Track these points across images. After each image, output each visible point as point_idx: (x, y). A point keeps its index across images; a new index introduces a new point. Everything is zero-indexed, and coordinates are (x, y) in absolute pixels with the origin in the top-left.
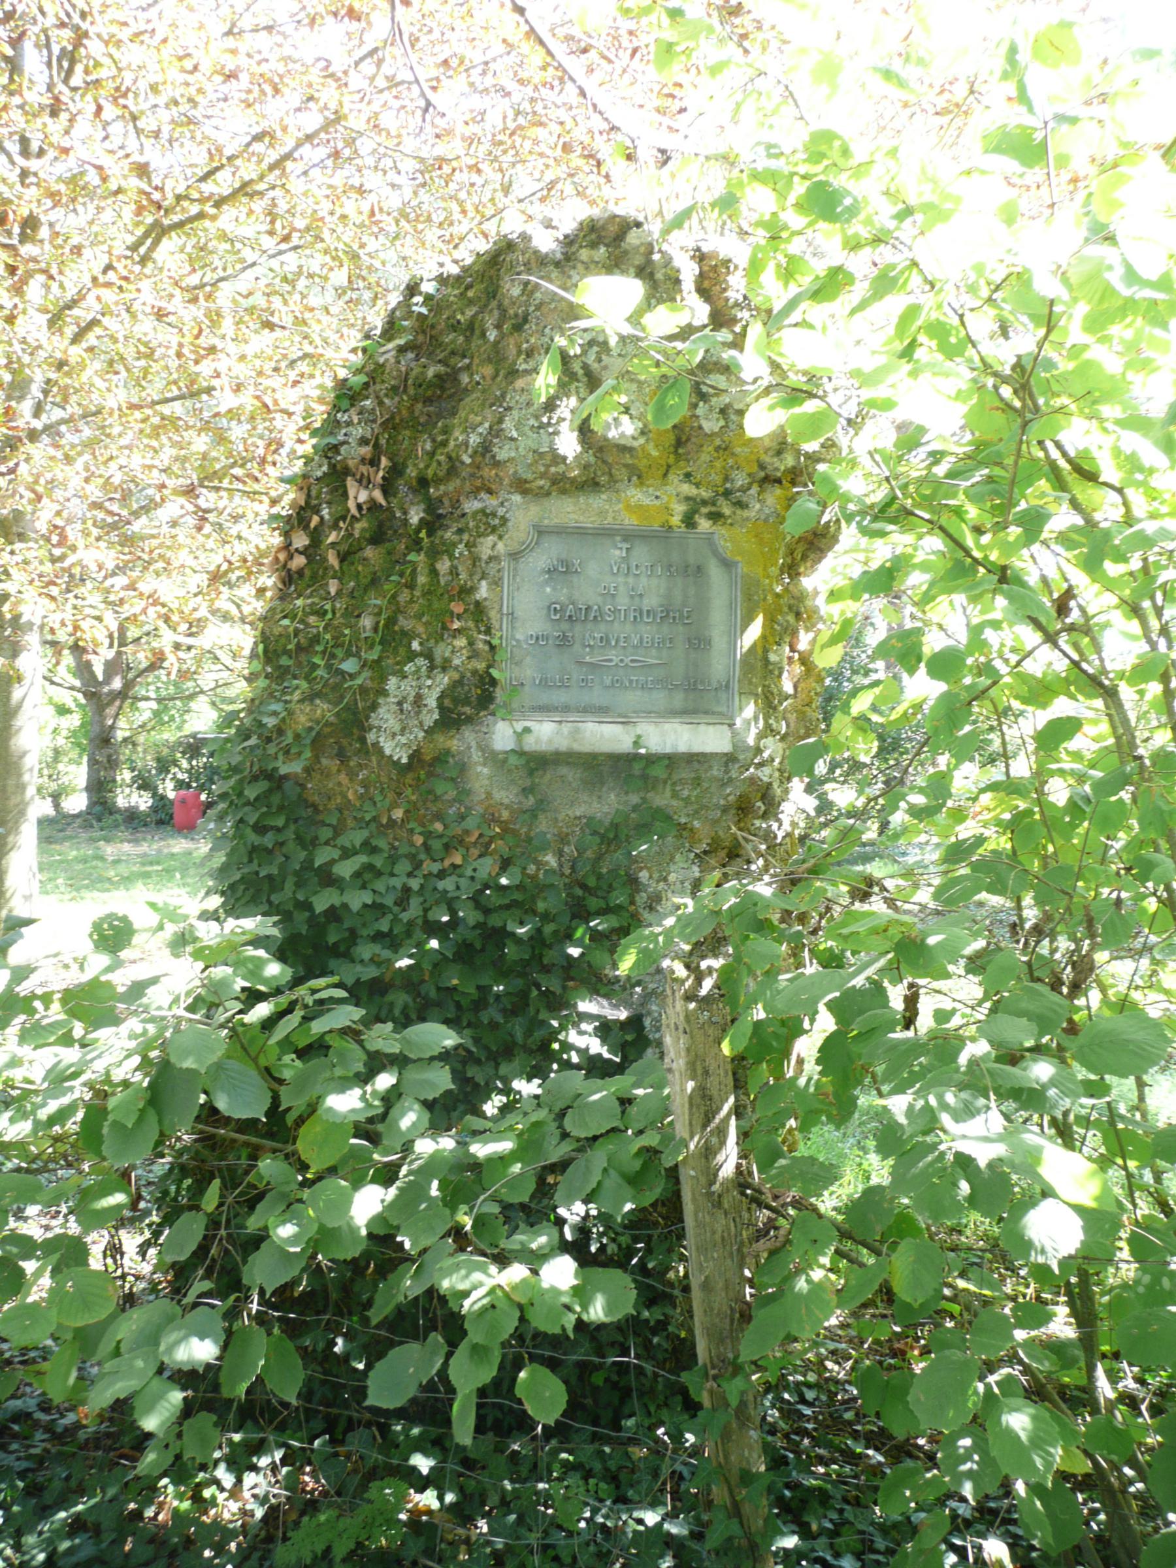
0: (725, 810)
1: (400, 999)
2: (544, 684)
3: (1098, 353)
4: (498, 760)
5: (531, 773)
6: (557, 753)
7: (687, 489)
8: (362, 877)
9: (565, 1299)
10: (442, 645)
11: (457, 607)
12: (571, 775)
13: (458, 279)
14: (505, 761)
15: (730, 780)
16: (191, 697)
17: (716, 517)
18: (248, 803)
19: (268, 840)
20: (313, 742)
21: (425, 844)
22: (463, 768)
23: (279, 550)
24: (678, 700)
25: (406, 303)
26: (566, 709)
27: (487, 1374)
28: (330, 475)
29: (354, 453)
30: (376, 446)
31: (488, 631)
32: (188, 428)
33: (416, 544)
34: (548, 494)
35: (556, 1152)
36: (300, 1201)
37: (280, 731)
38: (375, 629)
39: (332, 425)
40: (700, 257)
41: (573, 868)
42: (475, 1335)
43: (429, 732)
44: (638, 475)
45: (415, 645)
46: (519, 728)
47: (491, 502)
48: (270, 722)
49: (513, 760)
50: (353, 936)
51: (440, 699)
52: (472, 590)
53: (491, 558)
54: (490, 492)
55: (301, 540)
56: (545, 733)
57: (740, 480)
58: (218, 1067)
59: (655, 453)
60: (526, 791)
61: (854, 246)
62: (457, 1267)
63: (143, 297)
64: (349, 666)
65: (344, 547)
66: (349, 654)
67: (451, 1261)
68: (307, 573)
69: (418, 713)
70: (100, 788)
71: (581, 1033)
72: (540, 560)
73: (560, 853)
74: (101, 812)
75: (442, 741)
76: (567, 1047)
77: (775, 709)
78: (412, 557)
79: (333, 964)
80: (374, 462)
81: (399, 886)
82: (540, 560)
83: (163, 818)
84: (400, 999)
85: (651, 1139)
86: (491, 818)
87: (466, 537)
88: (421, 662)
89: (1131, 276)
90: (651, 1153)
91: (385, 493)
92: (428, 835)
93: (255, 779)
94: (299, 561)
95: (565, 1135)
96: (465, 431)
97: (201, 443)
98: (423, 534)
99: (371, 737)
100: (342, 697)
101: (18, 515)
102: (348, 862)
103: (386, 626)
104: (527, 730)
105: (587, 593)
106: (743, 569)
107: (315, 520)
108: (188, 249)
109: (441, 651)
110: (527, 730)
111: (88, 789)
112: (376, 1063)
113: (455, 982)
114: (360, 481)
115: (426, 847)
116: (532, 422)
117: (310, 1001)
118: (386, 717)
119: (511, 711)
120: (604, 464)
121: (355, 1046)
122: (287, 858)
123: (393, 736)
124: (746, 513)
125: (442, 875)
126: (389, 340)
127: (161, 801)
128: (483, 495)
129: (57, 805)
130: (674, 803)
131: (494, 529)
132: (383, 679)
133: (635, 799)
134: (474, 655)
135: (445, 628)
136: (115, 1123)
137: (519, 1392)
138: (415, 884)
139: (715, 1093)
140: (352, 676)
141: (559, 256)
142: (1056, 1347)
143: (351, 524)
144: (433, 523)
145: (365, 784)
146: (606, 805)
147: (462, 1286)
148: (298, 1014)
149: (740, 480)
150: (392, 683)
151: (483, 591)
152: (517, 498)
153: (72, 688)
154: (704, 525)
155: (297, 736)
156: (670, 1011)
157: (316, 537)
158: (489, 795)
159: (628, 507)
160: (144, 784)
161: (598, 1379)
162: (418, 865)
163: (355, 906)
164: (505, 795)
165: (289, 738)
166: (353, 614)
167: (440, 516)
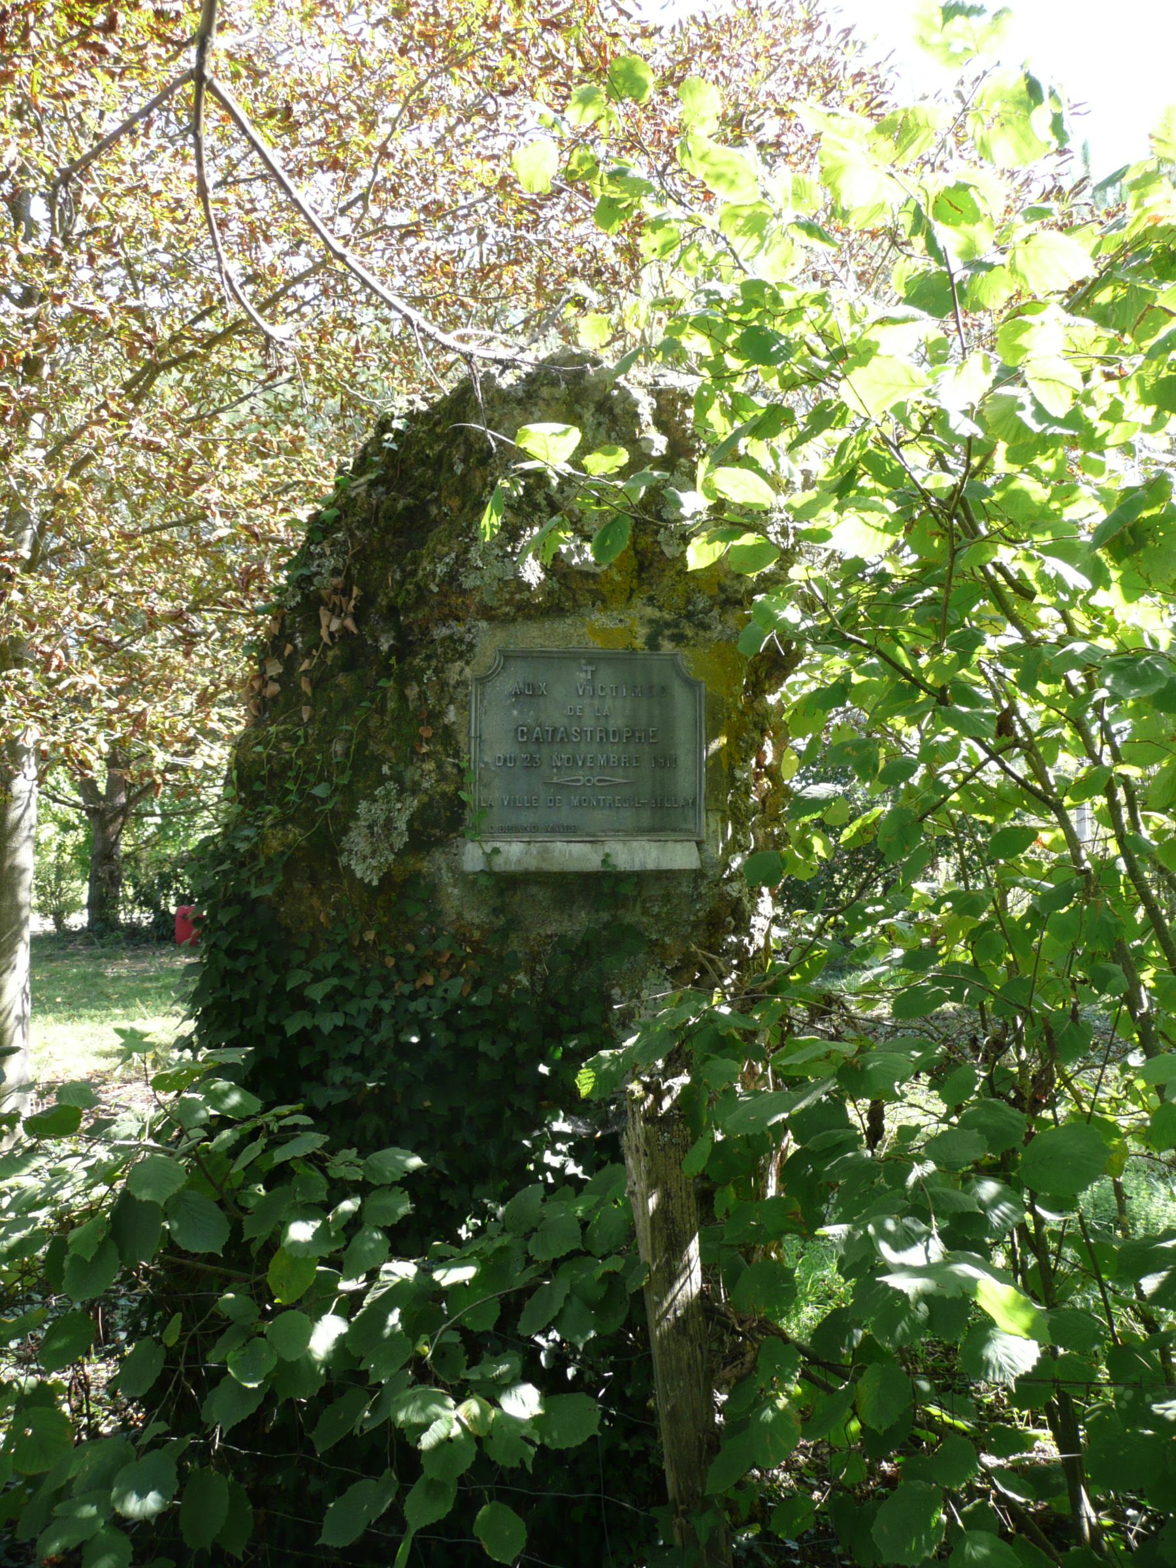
0: (695, 926)
1: (372, 1122)
2: (513, 805)
3: (1025, 483)
4: (469, 881)
5: (501, 893)
6: (527, 873)
7: (650, 612)
8: (333, 1000)
9: (524, 1432)
10: (411, 769)
11: (426, 732)
12: (541, 894)
13: (427, 415)
14: (474, 882)
15: (700, 896)
16: (194, 813)
17: (678, 638)
18: (221, 928)
19: (240, 965)
20: (285, 866)
21: (396, 965)
22: (434, 889)
23: (254, 678)
24: (646, 818)
25: (377, 439)
26: (534, 829)
27: (441, 1510)
28: (299, 609)
29: (326, 583)
30: (348, 576)
31: (456, 755)
32: (186, 551)
33: (386, 671)
34: (514, 620)
35: (520, 1278)
36: (262, 1335)
37: (253, 855)
38: (346, 754)
39: (306, 555)
40: (657, 392)
41: (545, 986)
42: (430, 1472)
43: (399, 854)
44: (601, 599)
45: (385, 769)
46: (488, 849)
47: (459, 629)
48: (242, 847)
49: (483, 881)
50: (325, 1061)
51: (410, 823)
52: (442, 713)
53: (458, 683)
54: (458, 619)
55: (275, 669)
56: (514, 853)
57: (702, 602)
58: (179, 1198)
59: (618, 578)
60: (496, 911)
61: (790, 384)
62: (414, 1398)
63: (135, 432)
64: (320, 791)
65: (317, 675)
66: (320, 779)
67: (410, 1392)
68: (281, 699)
69: (388, 836)
70: (102, 904)
71: (556, 1153)
72: (508, 683)
73: (532, 973)
74: (104, 929)
75: (411, 862)
76: (543, 1168)
77: (743, 824)
78: (383, 683)
79: (305, 1087)
80: (346, 592)
81: (370, 1008)
82: (508, 683)
83: (163, 933)
84: (372, 1122)
85: (615, 1264)
86: (461, 938)
87: (434, 663)
88: (391, 785)
89: (1041, 414)
90: (611, 1278)
91: (357, 621)
92: (399, 957)
93: (228, 903)
94: (273, 688)
95: (529, 1261)
96: (432, 561)
97: (197, 567)
98: (393, 661)
99: (343, 860)
100: (314, 822)
101: (16, 642)
102: (320, 985)
103: (357, 751)
104: (496, 851)
105: (554, 716)
106: (706, 688)
107: (289, 648)
108: (186, 383)
109: (412, 774)
110: (496, 851)
111: (89, 906)
112: (341, 1190)
113: (427, 1104)
114: (332, 611)
115: (398, 968)
116: (497, 551)
117: (275, 1127)
118: (357, 840)
119: (480, 832)
120: (568, 588)
121: (317, 1174)
122: (259, 981)
123: (364, 861)
124: (708, 635)
125: (413, 996)
126: (361, 475)
127: (162, 915)
128: (453, 623)
129: (58, 922)
130: (645, 919)
131: (461, 655)
132: (355, 804)
133: (605, 916)
134: (443, 777)
135: (414, 752)
136: (76, 1257)
137: (476, 1531)
138: (386, 1006)
139: (678, 1216)
140: (324, 801)
141: (521, 394)
142: (1033, 1477)
143: (324, 652)
144: (402, 650)
145: (337, 907)
146: (578, 922)
147: (417, 1419)
148: (262, 1141)
149: (702, 602)
150: (363, 806)
151: (451, 715)
152: (483, 624)
153: (76, 805)
154: (667, 646)
155: (269, 861)
156: (631, 1133)
157: (290, 664)
158: (460, 916)
159: (594, 632)
160: (147, 899)
161: (578, 1515)
162: (389, 987)
163: (327, 1028)
164: (475, 916)
165: (262, 863)
166: (324, 740)
167: (411, 643)
